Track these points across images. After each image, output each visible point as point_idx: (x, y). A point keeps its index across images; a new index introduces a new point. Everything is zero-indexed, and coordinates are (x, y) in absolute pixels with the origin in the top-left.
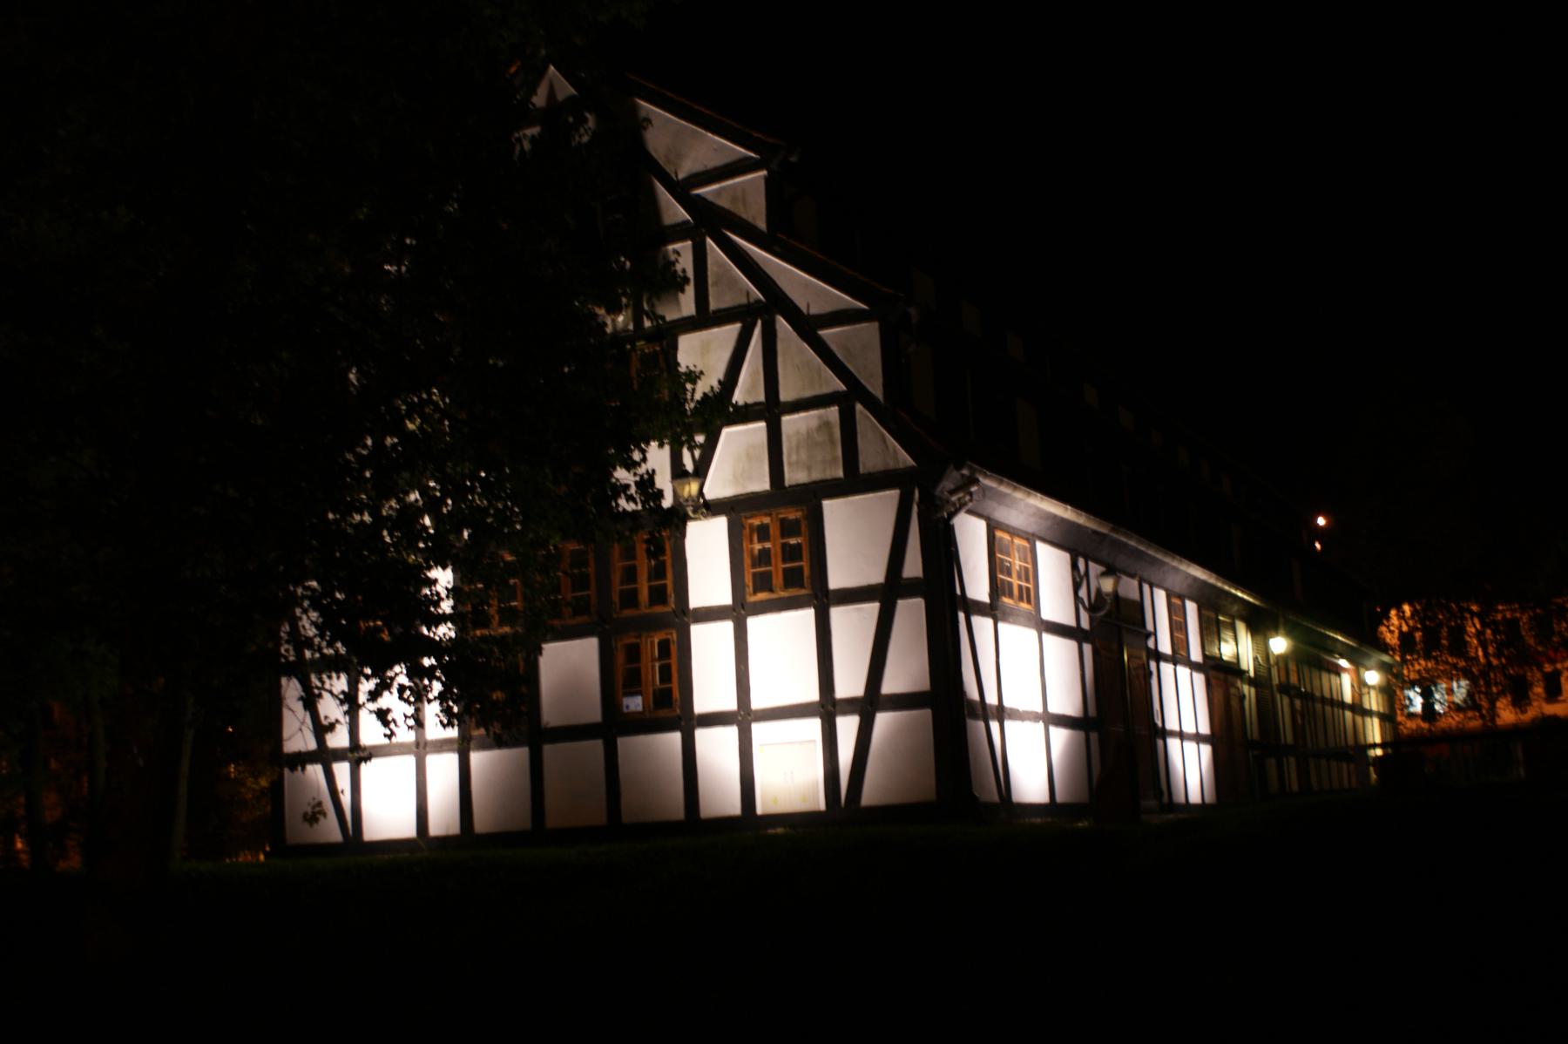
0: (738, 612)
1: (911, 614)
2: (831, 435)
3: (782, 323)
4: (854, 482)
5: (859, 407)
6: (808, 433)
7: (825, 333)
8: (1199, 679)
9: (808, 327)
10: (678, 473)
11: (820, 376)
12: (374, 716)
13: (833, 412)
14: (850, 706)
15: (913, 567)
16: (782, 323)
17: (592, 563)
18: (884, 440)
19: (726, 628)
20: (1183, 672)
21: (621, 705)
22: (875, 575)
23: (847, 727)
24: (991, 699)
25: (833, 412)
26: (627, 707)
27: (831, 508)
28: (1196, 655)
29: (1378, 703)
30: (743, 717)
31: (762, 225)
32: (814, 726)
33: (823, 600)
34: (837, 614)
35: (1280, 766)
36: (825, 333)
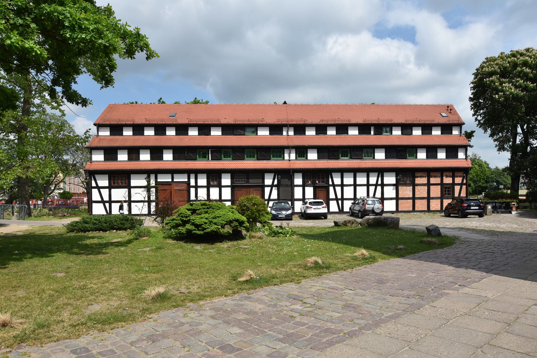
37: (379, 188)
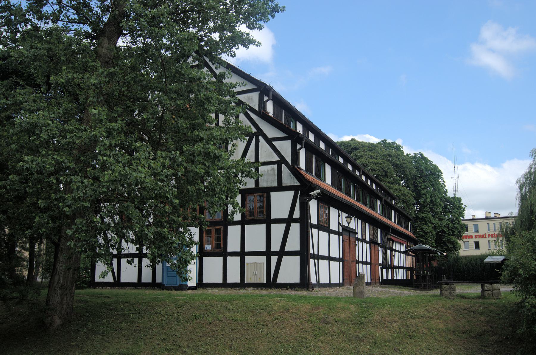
0: (243, 223)
1: (295, 228)
2: (274, 173)
3: (261, 138)
4: (281, 188)
5: (283, 165)
6: (267, 171)
7: (274, 143)
8: (368, 245)
9: (269, 141)
10: (157, 171)
11: (272, 154)
12: (248, 32)
13: (275, 166)
14: (275, 253)
15: (297, 214)
16: (261, 138)
17: (222, 233)
18: (291, 176)
19: (239, 227)
20: (364, 244)
21: (204, 248)
22: (286, 216)
23: (274, 259)
24: (316, 253)
25: (275, 166)
26: (207, 248)
27: (273, 195)
28: (368, 239)
29: (510, 287)
30: (242, 254)
31: (257, 109)
32: (263, 259)
33: (268, 221)
34: (273, 226)
35: (387, 272)
36: (274, 143)
37: (275, 246)
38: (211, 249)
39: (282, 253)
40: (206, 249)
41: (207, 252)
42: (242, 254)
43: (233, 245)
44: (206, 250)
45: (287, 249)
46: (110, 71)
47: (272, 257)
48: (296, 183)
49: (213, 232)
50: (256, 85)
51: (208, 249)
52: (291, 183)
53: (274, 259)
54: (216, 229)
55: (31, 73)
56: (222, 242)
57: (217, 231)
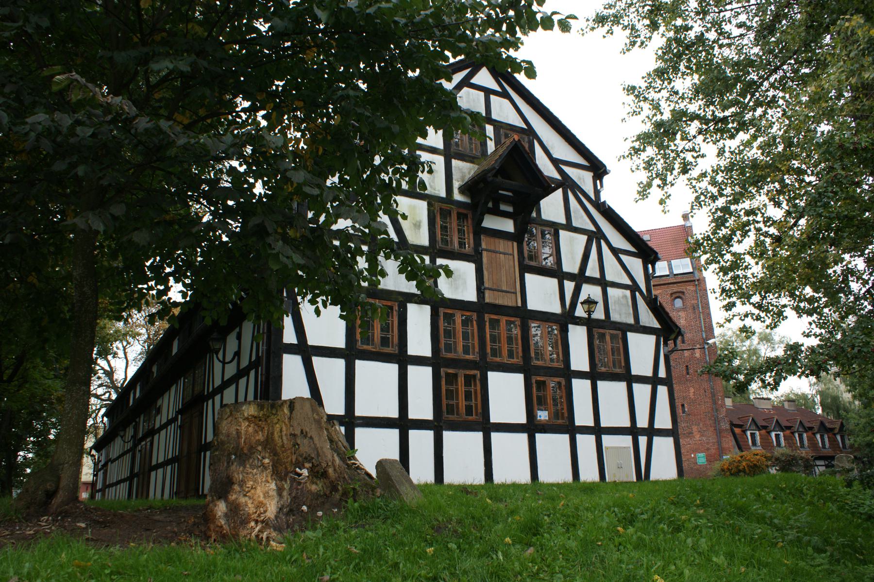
2: (627, 302)
22: (313, 340)
26: (540, 416)
37: (642, 422)
38: (547, 418)
39: (651, 432)
40: (539, 418)
41: (540, 425)
42: (597, 431)
43: (583, 416)
44: (540, 421)
45: (316, 361)
46: (101, 182)
47: (640, 438)
48: (656, 325)
49: (461, 380)
50: (486, 113)
51: (542, 418)
52: (649, 323)
53: (643, 440)
54: (466, 376)
55: (100, 354)
56: (444, 387)
57: (469, 380)
